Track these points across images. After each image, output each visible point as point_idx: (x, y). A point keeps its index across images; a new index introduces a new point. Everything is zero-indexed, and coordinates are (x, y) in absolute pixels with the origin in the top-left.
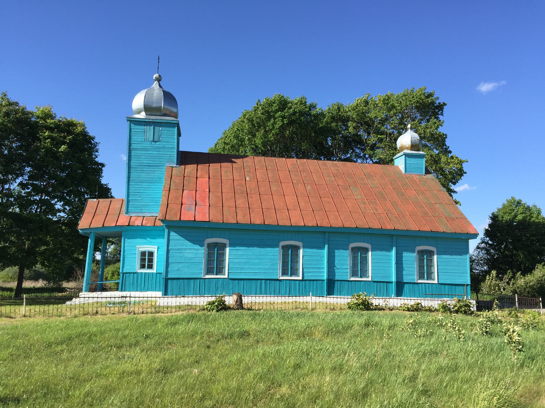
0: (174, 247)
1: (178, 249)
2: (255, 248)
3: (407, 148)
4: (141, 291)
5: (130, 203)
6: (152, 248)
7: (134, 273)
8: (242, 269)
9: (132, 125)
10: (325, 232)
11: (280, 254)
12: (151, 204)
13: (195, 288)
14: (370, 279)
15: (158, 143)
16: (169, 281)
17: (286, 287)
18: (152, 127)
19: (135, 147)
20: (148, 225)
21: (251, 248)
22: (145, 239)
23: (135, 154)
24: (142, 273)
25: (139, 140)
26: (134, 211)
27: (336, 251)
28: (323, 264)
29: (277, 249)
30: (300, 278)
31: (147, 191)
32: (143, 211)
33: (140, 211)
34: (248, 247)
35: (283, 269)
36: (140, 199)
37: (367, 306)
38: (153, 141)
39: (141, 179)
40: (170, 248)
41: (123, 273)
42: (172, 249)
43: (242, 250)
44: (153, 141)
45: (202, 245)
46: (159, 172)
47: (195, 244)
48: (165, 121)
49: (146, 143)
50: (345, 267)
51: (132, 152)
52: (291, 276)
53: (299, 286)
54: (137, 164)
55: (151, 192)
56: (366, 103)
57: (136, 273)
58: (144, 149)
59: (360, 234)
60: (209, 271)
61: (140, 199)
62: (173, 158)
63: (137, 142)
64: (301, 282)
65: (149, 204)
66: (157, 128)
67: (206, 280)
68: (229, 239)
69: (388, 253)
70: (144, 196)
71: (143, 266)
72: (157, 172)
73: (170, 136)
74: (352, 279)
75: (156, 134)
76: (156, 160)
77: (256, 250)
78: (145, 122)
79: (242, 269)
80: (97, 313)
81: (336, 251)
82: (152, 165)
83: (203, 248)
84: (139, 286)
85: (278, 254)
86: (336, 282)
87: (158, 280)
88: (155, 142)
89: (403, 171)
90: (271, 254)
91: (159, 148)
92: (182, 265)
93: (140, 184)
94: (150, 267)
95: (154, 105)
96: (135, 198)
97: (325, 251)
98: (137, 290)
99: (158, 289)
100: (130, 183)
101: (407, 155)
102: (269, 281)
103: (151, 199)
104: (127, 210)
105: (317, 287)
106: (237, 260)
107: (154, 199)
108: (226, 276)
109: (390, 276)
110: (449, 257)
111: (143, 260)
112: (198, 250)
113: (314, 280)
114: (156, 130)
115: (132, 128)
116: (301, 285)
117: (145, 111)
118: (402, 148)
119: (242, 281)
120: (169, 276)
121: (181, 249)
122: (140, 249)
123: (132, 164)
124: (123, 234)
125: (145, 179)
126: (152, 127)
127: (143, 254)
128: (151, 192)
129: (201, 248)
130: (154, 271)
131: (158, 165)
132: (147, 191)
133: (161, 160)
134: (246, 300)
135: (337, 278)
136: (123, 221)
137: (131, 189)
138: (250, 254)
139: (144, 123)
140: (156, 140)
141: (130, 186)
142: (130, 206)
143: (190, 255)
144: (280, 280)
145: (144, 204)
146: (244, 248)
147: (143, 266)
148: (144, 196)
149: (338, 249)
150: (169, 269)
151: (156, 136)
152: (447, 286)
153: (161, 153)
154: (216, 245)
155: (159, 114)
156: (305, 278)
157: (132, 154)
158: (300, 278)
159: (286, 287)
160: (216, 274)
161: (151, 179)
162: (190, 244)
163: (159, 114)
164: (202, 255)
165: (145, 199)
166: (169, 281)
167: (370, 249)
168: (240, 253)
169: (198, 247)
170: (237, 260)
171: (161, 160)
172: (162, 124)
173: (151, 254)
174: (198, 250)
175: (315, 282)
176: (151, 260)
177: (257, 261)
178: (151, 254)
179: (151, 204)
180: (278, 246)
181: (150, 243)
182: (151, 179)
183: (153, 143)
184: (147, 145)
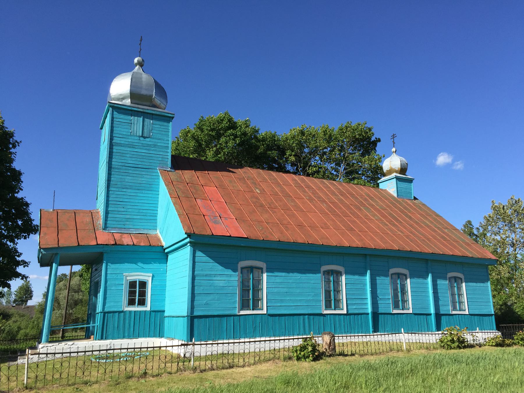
0: (201, 273)
1: (206, 275)
2: (296, 274)
3: (396, 172)
4: (129, 337)
5: (110, 215)
6: (146, 277)
7: (120, 312)
8: (282, 301)
9: (115, 113)
10: (366, 255)
11: (322, 281)
12: (138, 217)
13: (228, 328)
14: (411, 311)
15: (147, 139)
16: (196, 320)
17: (331, 326)
18: (141, 119)
19: (118, 142)
20: (142, 244)
21: (291, 274)
22: (136, 263)
23: (118, 151)
24: (130, 312)
25: (125, 133)
26: (115, 226)
27: (377, 278)
28: (366, 294)
29: (319, 276)
30: (345, 312)
31: (132, 201)
32: (126, 226)
33: (123, 227)
34: (288, 272)
35: (326, 300)
36: (123, 210)
37: (462, 344)
38: (142, 136)
39: (124, 184)
40: (196, 273)
41: (104, 313)
42: (199, 275)
43: (281, 277)
44: (142, 136)
45: (235, 270)
46: (148, 177)
47: (226, 268)
48: (158, 113)
49: (133, 138)
50: (387, 297)
51: (114, 147)
52: (335, 309)
53: (344, 322)
54: (120, 164)
55: (137, 201)
56: (302, 133)
57: (122, 312)
58: (132, 146)
59: (399, 258)
60: (244, 305)
61: (123, 210)
62: (167, 160)
63: (120, 136)
64: (345, 316)
65: (135, 217)
66: (147, 120)
67: (241, 317)
68: (266, 262)
69: (425, 281)
70: (129, 207)
71: (131, 302)
72: (145, 176)
73: (163, 133)
74: (395, 311)
75: (145, 127)
76: (145, 160)
77: (296, 276)
78: (132, 110)
79: (282, 301)
80: (145, 373)
81: (377, 278)
82: (139, 166)
83: (237, 273)
84: (126, 329)
85: (320, 281)
86: (380, 316)
87: (127, 322)
88: (145, 138)
89: (395, 195)
90: (312, 282)
91: (148, 145)
92: (211, 297)
93: (124, 190)
94: (142, 303)
95: (144, 92)
96: (116, 209)
97: (368, 278)
98: (124, 337)
99: (152, 333)
100: (111, 189)
101: (397, 178)
102: (312, 317)
103: (137, 211)
104: (106, 224)
105: (362, 323)
106: (276, 290)
107: (141, 211)
108: (264, 312)
109: (428, 308)
110: (474, 284)
111: (132, 293)
112: (231, 276)
113: (358, 314)
114: (146, 123)
115: (115, 116)
116: (346, 320)
117: (131, 98)
118: (390, 172)
119: (284, 318)
120: (196, 313)
121: (210, 275)
122: (128, 278)
123: (113, 163)
124: (105, 256)
125: (131, 184)
126: (141, 119)
127: (132, 284)
128: (137, 201)
129: (234, 273)
130: (148, 308)
131: (147, 167)
132: (132, 201)
133: (151, 161)
134: (338, 341)
135: (381, 311)
136: (103, 238)
137: (111, 196)
138: (291, 281)
139: (131, 112)
140: (145, 135)
141: (110, 192)
142: (109, 219)
143: (222, 284)
144: (324, 315)
145: (128, 217)
146: (283, 274)
147: (131, 302)
148: (129, 207)
149: (379, 276)
150: (196, 303)
151: (145, 131)
152: (476, 317)
153: (151, 152)
154: (251, 269)
155: (148, 104)
156: (350, 312)
157: (114, 151)
158: (345, 312)
159: (331, 326)
160: (253, 309)
161: (138, 185)
162: (221, 268)
163: (148, 104)
164: (236, 284)
165: (130, 210)
166: (196, 320)
167: (408, 276)
168: (278, 280)
169: (230, 272)
170: (276, 290)
171: (151, 161)
172: (154, 116)
173: (143, 284)
174: (231, 276)
175: (359, 316)
176: (143, 294)
177: (298, 291)
178: (143, 284)
179: (138, 217)
180: (319, 272)
181: (142, 270)
182: (138, 185)
183: (142, 139)
184: (134, 140)
